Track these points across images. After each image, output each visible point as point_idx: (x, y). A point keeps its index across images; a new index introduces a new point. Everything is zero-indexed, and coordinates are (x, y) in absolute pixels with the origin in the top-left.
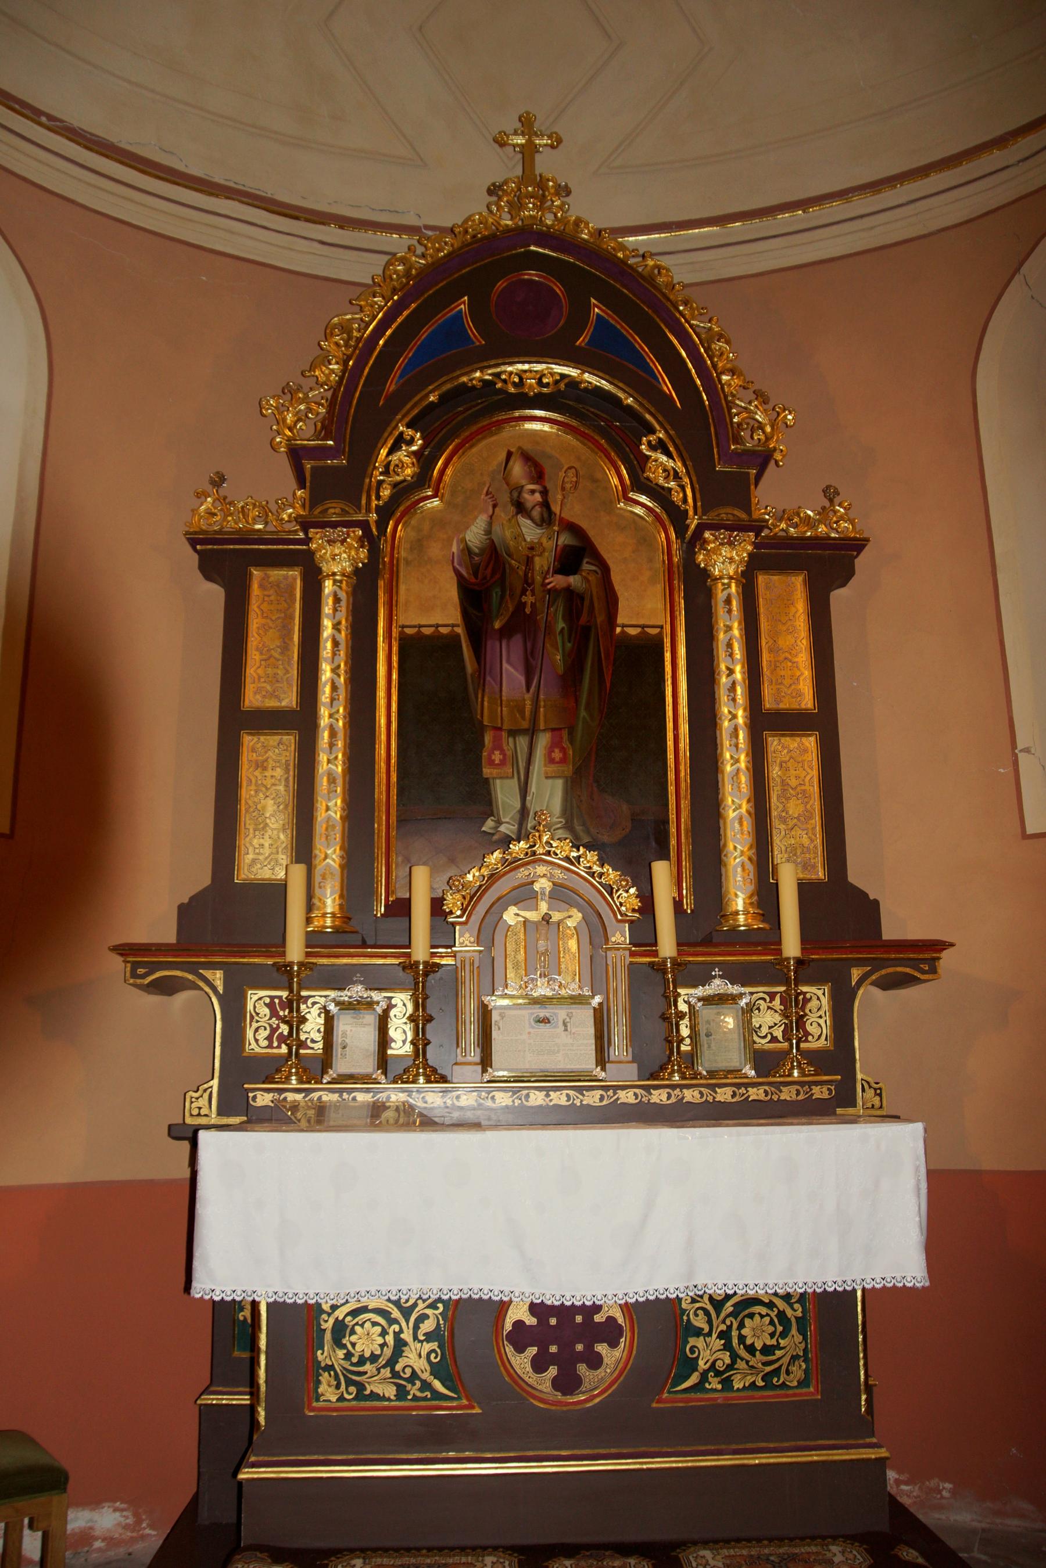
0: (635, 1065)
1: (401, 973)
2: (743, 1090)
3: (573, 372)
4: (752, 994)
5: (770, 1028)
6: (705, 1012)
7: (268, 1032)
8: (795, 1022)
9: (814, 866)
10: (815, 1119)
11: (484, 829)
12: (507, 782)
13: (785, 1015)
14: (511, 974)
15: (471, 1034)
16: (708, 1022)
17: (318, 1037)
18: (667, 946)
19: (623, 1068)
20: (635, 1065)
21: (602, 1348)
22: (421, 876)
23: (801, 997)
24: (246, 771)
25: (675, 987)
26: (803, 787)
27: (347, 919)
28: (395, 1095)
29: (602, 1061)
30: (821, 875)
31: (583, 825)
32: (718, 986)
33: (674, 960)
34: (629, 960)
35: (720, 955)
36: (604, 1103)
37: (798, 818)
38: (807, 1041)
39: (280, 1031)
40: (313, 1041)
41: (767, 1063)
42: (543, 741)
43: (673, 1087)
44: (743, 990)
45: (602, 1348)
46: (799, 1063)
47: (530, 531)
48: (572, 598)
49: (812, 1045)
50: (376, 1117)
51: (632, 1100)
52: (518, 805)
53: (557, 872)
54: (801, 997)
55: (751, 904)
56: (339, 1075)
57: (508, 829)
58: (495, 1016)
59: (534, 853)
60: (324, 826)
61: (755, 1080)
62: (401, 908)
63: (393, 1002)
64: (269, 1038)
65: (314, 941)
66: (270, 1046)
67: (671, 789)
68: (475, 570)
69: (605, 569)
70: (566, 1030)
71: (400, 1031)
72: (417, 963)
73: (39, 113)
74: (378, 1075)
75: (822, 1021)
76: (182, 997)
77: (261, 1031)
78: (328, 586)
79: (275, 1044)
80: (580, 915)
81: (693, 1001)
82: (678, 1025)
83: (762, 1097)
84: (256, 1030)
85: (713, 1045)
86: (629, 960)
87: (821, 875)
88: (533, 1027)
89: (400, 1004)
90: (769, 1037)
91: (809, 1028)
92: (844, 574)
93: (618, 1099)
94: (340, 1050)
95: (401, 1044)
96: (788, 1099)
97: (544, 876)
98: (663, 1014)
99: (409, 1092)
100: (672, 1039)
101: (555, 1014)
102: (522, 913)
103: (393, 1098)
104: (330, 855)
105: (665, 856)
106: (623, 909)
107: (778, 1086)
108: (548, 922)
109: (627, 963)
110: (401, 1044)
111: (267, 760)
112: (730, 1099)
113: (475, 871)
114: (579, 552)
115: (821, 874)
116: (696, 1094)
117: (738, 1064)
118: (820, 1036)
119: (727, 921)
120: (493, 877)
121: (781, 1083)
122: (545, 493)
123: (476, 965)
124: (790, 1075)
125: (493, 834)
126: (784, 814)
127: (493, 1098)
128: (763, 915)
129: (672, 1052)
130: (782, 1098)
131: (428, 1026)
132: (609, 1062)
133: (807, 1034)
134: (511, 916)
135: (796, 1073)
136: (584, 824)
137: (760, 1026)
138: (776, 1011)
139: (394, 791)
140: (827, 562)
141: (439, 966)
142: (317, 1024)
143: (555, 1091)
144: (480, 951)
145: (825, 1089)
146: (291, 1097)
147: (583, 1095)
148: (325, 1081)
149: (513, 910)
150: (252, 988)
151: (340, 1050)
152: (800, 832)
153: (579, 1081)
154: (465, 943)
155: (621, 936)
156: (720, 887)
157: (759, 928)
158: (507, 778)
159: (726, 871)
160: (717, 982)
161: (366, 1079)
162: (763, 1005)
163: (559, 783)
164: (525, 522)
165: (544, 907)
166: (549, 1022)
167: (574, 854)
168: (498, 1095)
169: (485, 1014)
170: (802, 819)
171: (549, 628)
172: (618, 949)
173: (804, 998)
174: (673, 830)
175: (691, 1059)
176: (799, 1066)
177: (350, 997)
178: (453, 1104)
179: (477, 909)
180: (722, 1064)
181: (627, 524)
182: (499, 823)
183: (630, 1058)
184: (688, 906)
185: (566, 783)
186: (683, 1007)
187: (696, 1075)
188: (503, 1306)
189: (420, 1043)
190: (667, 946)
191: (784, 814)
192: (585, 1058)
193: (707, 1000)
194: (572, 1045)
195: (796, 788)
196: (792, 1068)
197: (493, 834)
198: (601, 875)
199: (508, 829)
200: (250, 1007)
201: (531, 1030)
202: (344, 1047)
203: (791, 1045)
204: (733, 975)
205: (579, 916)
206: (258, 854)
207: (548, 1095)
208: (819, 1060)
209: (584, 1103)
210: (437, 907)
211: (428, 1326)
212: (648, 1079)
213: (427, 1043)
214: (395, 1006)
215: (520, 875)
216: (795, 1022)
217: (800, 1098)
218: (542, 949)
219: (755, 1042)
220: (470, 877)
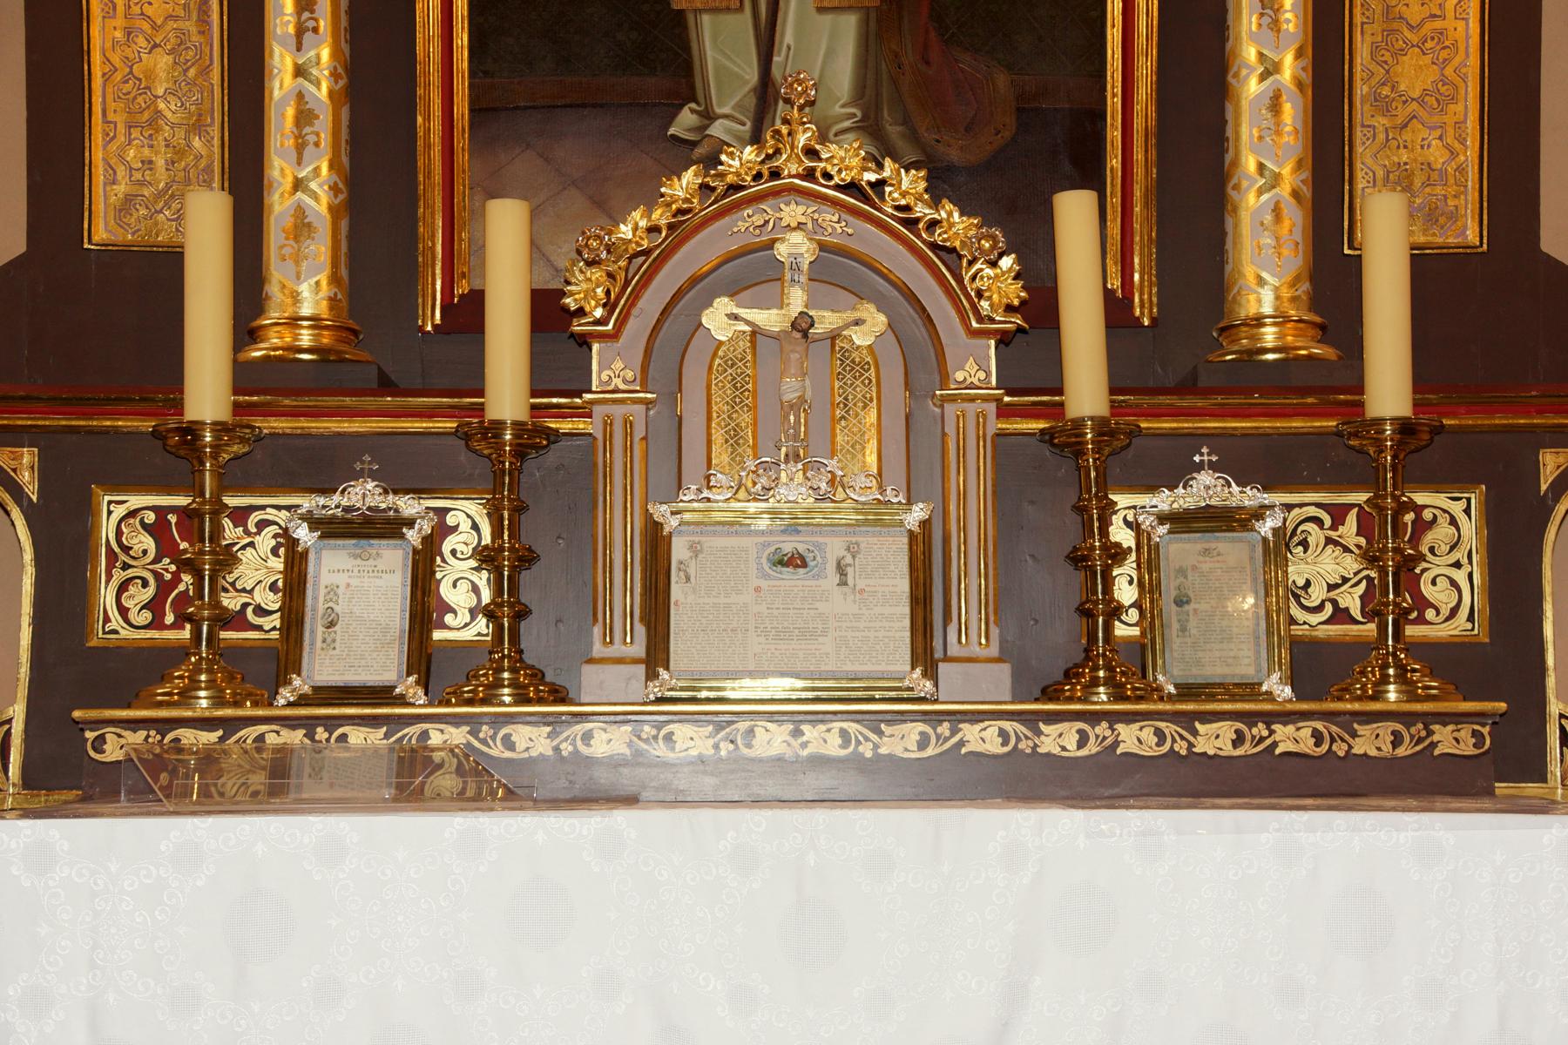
0: (1006, 668)
1: (464, 456)
2: (1260, 729)
4: (1289, 507)
5: (1331, 587)
6: (1174, 547)
7: (151, 591)
8: (1395, 572)
9: (1453, 216)
10: (1439, 802)
11: (671, 131)
12: (730, 20)
13: (1371, 558)
14: (721, 456)
15: (625, 595)
16: (1182, 572)
17: (272, 601)
18: (1086, 390)
19: (978, 675)
20: (1006, 668)
22: (506, 227)
23: (1409, 517)
25: (1104, 485)
26: (1438, 24)
27: (348, 332)
29: (925, 656)
30: (1472, 236)
31: (894, 109)
32: (1206, 488)
33: (1101, 425)
34: (995, 425)
35: (1214, 415)
36: (930, 751)
37: (1420, 101)
38: (1420, 620)
39: (182, 587)
40: (261, 611)
41: (1318, 668)
43: (1094, 718)
44: (1268, 498)
46: (1402, 669)
51: (994, 746)
52: (752, 76)
53: (830, 217)
54: (1409, 517)
55: (1294, 299)
56: (316, 689)
57: (728, 131)
58: (679, 550)
59: (775, 174)
60: (290, 112)
61: (1289, 707)
63: (450, 520)
64: (155, 605)
65: (255, 382)
66: (157, 623)
67: (1114, 35)
70: (843, 583)
71: (464, 586)
72: (498, 426)
74: (409, 686)
75: (1460, 576)
77: (132, 589)
79: (170, 618)
80: (882, 318)
81: (1147, 521)
82: (1108, 582)
83: (1307, 745)
84: (123, 588)
85: (1192, 624)
86: (995, 425)
87: (1472, 236)
88: (766, 576)
89: (465, 525)
90: (1329, 608)
91: (1427, 590)
93: (962, 743)
94: (320, 629)
95: (464, 625)
96: (1373, 752)
97: (800, 226)
98: (1075, 549)
99: (473, 722)
100: (1096, 609)
101: (818, 546)
102: (742, 312)
103: (436, 739)
104: (305, 181)
105: (1089, 175)
106: (985, 304)
107: (1349, 722)
108: (805, 335)
109: (991, 431)
110: (464, 625)
112: (1229, 750)
113: (638, 217)
115: (1471, 233)
116: (1148, 735)
117: (1251, 671)
118: (1454, 612)
119: (1236, 341)
120: (682, 227)
121: (1354, 714)
123: (639, 432)
124: (1378, 696)
125: (694, 144)
126: (1386, 91)
127: (669, 738)
128: (1322, 327)
129: (1092, 638)
130: (1357, 750)
131: (525, 576)
132: (947, 659)
133: (1422, 603)
134: (719, 319)
135: (1392, 693)
136: (906, 121)
137: (1308, 584)
138: (1346, 549)
139: (462, 39)
141: (554, 436)
142: (270, 570)
143: (813, 723)
144: (648, 403)
145: (1465, 733)
146: (188, 736)
147: (880, 733)
148: (282, 702)
149: (723, 305)
150: (111, 491)
151: (320, 629)
152: (1425, 133)
153: (871, 700)
155: (976, 368)
156: (1222, 263)
157: (1310, 357)
158: (728, 10)
159: (1236, 226)
160: (1205, 478)
161: (382, 694)
162: (1315, 535)
165: (797, 299)
166: (804, 565)
167: (871, 177)
168: (681, 731)
169: (656, 543)
170: (1432, 101)
172: (972, 399)
173: (1418, 520)
174: (1114, 134)
175: (1142, 653)
176: (1402, 678)
177: (347, 509)
178: (576, 752)
179: (641, 304)
180: (1213, 668)
182: (708, 116)
183: (994, 651)
184: (1143, 309)
185: (865, 25)
186: (1121, 535)
187: (1155, 692)
189: (507, 612)
190: (1086, 390)
191: (1386, 91)
192: (890, 650)
193: (1181, 521)
194: (857, 617)
195: (1420, 25)
196: (1385, 679)
197: (694, 144)
198: (933, 224)
199: (728, 131)
200: (107, 529)
201: (764, 584)
202: (331, 624)
203: (1382, 628)
205: (877, 321)
206: (141, 183)
207: (797, 733)
208: (1451, 664)
209: (883, 751)
212: (1037, 700)
213: (521, 614)
214: (455, 529)
215: (742, 226)
216: (1395, 572)
217: (1402, 751)
218: (790, 396)
219: (1292, 621)
220: (625, 231)
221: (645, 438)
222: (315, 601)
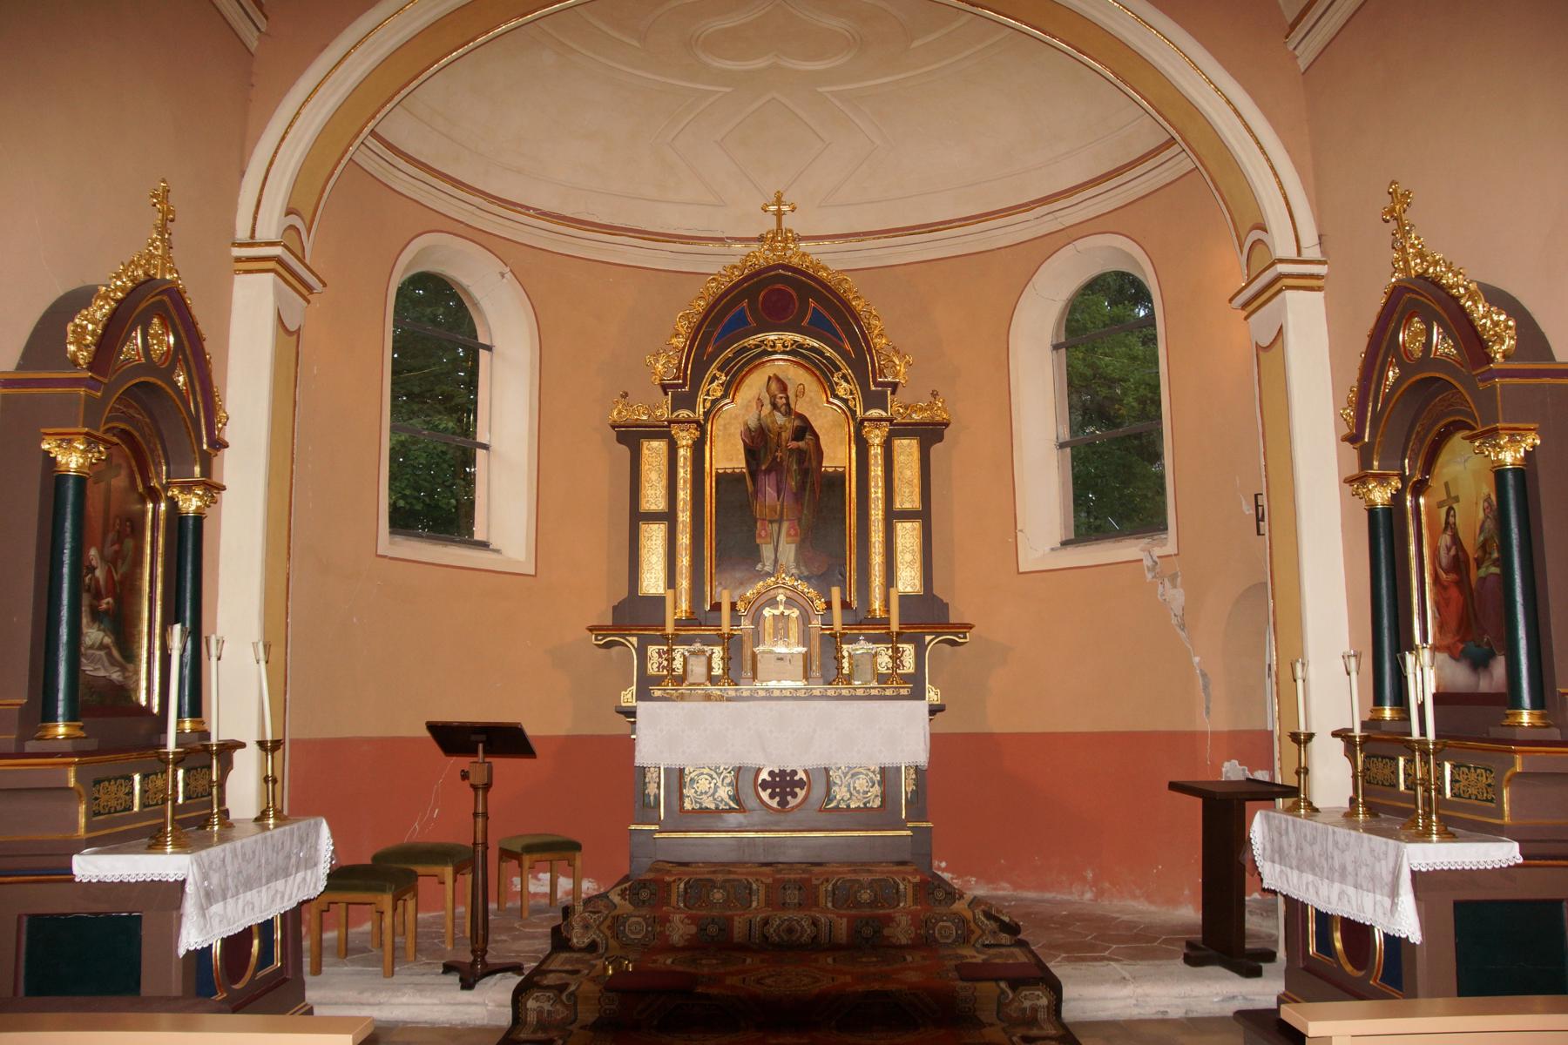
3: (798, 338)
8: (896, 657)
18: (838, 626)
21: (797, 790)
24: (643, 541)
28: (715, 690)
42: (785, 525)
45: (797, 790)
47: (780, 419)
48: (801, 455)
49: (906, 671)
50: (708, 697)
62: (717, 607)
65: (678, 623)
68: (752, 439)
69: (817, 437)
73: (528, 208)
76: (616, 649)
78: (681, 452)
92: (939, 438)
95: (717, 671)
104: (684, 583)
110: (717, 671)
111: (653, 536)
114: (804, 429)
120: (760, 594)
122: (787, 398)
134: (767, 612)
140: (929, 434)
154: (746, 624)
155: (816, 623)
163: (793, 546)
164: (777, 414)
165: (781, 608)
169: (754, 656)
171: (789, 470)
181: (826, 415)
188: (759, 770)
189: (726, 670)
190: (838, 626)
204: (869, 639)
208: (906, 678)
210: (733, 606)
211: (728, 780)
216: (896, 657)
221: (638, 517)
222: (689, 668)
